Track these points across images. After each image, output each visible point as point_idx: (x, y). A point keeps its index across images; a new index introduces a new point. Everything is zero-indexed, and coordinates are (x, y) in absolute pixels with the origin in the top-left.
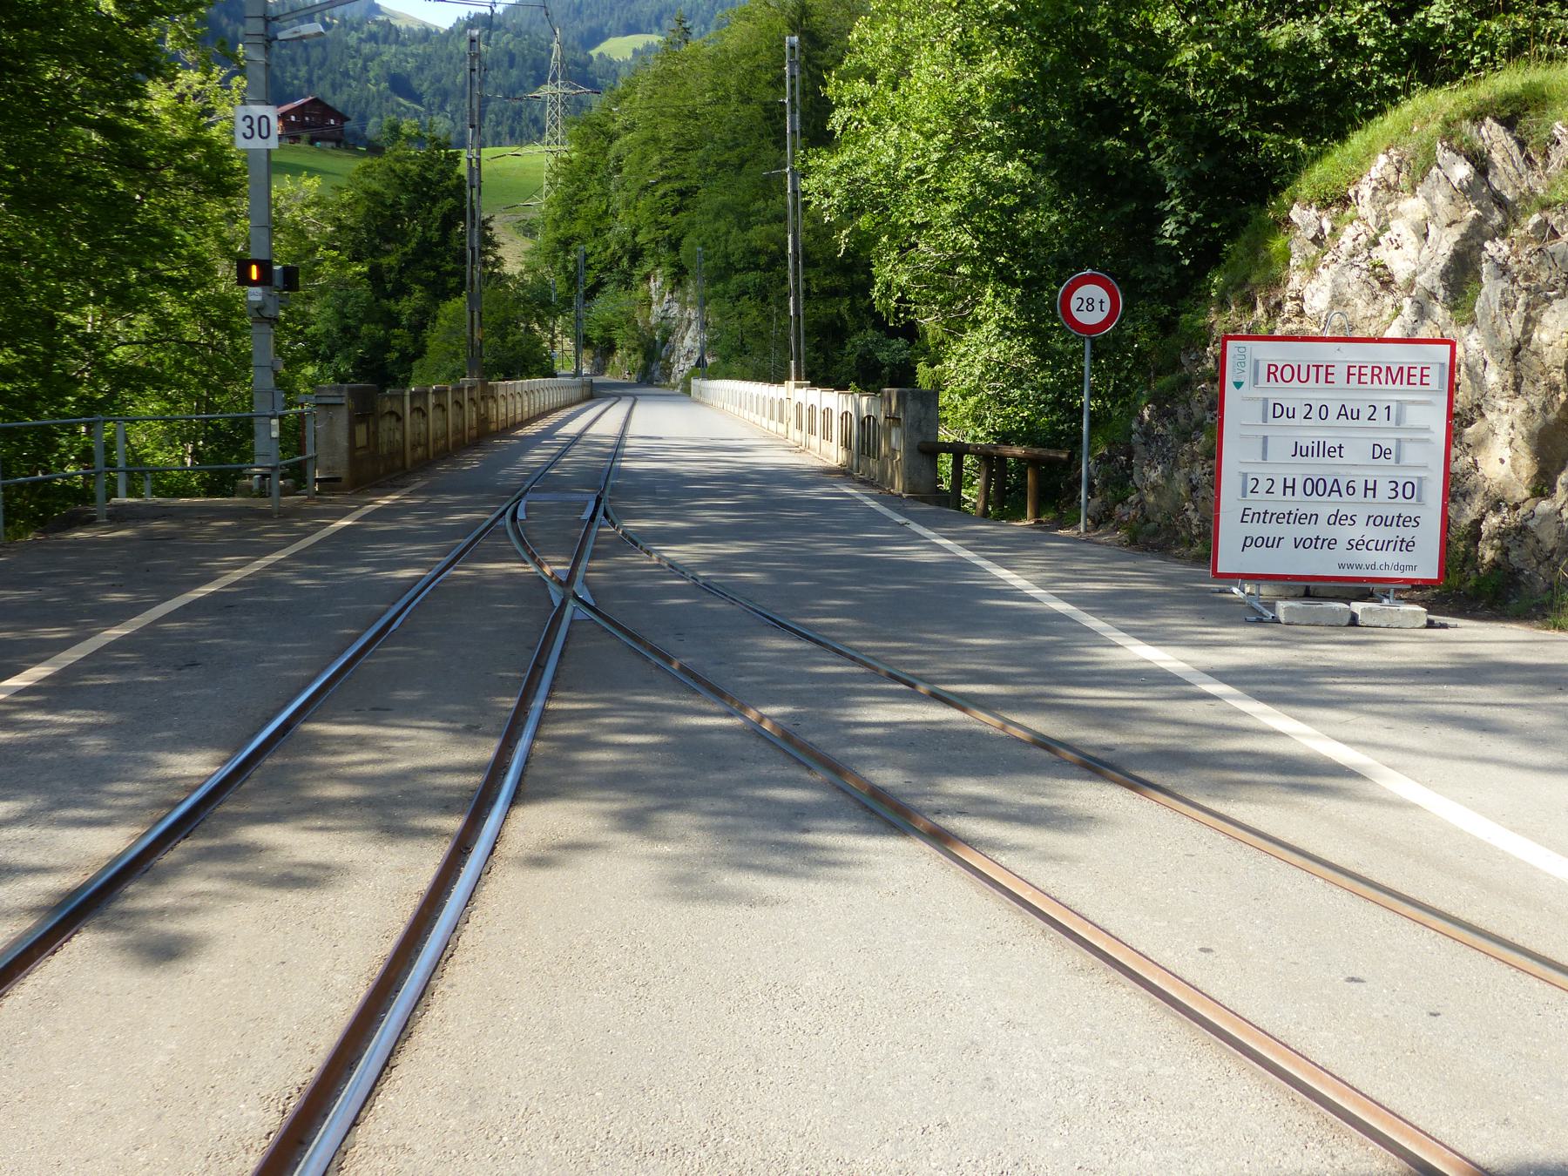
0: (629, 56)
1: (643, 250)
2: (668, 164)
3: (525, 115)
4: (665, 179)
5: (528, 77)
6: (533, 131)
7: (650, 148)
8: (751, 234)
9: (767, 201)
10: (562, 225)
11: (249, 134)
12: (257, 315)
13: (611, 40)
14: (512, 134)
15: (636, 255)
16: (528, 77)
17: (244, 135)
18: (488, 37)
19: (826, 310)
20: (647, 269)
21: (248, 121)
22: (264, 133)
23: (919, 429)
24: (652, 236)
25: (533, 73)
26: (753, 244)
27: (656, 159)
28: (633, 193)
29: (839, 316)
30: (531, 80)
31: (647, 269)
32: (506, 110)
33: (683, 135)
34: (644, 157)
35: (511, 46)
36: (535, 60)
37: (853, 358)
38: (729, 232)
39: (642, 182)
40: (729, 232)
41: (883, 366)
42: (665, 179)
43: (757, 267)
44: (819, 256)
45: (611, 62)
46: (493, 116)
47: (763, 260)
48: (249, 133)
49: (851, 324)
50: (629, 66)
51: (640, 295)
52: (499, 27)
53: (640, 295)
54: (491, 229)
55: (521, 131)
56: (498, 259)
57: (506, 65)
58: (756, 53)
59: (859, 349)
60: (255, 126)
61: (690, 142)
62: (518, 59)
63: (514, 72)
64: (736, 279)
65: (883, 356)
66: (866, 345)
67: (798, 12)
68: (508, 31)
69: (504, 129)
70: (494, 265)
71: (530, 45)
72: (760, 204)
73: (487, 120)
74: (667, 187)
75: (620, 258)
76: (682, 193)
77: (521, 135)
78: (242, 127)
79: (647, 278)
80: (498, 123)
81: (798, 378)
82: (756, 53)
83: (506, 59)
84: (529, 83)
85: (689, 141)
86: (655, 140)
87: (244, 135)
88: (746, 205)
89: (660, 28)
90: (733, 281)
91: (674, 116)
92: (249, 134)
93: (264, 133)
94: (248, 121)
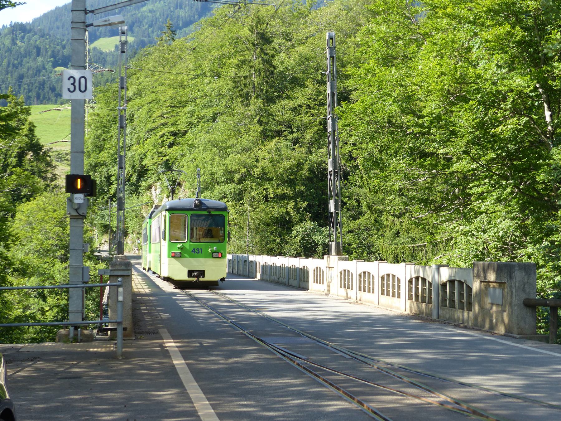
0: (113, 49)
1: (148, 170)
2: (165, 116)
3: (47, 86)
4: (164, 125)
5: (48, 62)
6: (52, 95)
7: (154, 106)
8: (227, 161)
9: (237, 139)
10: (92, 155)
11: (72, 89)
12: (75, 213)
13: (101, 39)
14: (38, 97)
15: (142, 172)
16: (48, 62)
17: (69, 90)
18: (23, 38)
19: (277, 210)
20: (149, 182)
21: (72, 80)
22: (83, 88)
23: (524, 290)
24: (155, 161)
25: (52, 59)
26: (230, 167)
27: (158, 113)
28: (142, 134)
29: (287, 213)
30: (51, 64)
31: (149, 182)
32: (35, 83)
33: (175, 98)
34: (150, 112)
35: (38, 43)
36: (53, 51)
37: (298, 240)
38: (213, 159)
39: (148, 127)
40: (213, 159)
41: (317, 245)
42: (164, 125)
43: (233, 181)
44: (273, 174)
45: (101, 53)
46: (26, 86)
47: (237, 177)
48: (72, 88)
49: (296, 217)
50: (113, 55)
51: (145, 199)
52: (30, 31)
53: (145, 199)
54: (50, 156)
55: (44, 96)
56: (55, 175)
57: (35, 54)
58: (222, 47)
59: (301, 233)
60: (77, 84)
61: (180, 102)
62: (43, 51)
63: (40, 59)
64: (218, 189)
65: (317, 238)
66: (305, 231)
67: (255, 21)
68: (36, 34)
69: (33, 94)
70: (52, 180)
71: (50, 42)
72: (233, 141)
73: (22, 89)
74: (165, 130)
75: (131, 175)
76: (174, 134)
77: (44, 98)
78: (67, 84)
79: (150, 187)
80: (30, 91)
81: (338, 253)
82: (222, 47)
83: (35, 51)
84: (49, 66)
85: (179, 101)
86: (158, 101)
87: (69, 90)
88: (224, 142)
89: (133, 32)
90: (216, 191)
91: (170, 86)
92: (72, 89)
93: (83, 88)
94: (72, 80)
